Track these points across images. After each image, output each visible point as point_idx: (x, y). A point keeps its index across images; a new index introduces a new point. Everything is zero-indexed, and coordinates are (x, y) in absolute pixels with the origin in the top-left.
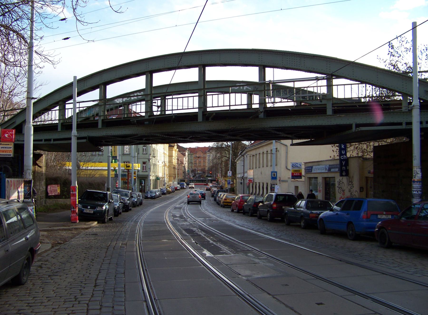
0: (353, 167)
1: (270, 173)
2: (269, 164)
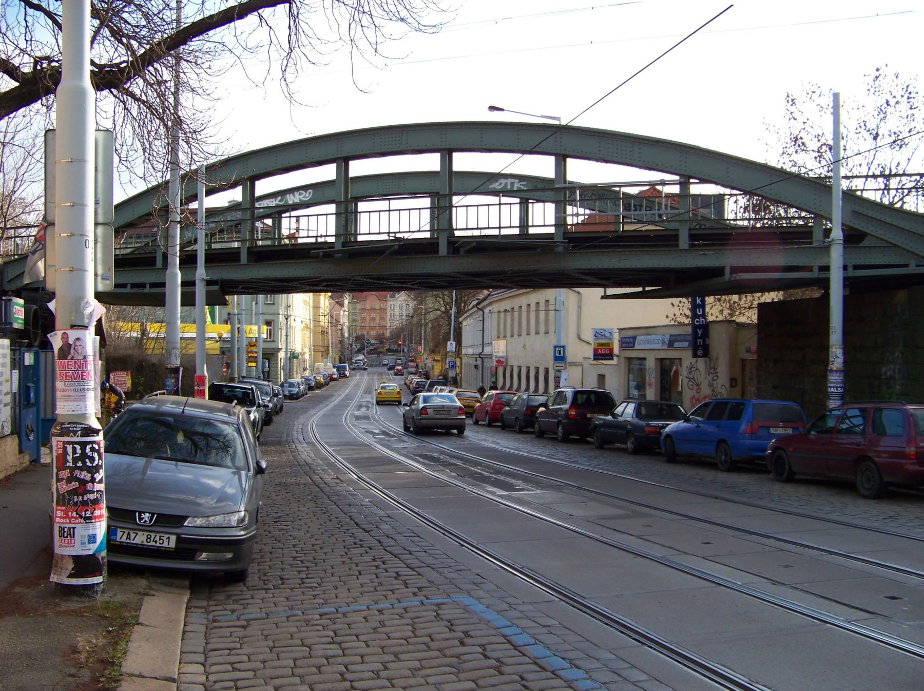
0: (719, 341)
1: (552, 349)
2: (542, 329)
